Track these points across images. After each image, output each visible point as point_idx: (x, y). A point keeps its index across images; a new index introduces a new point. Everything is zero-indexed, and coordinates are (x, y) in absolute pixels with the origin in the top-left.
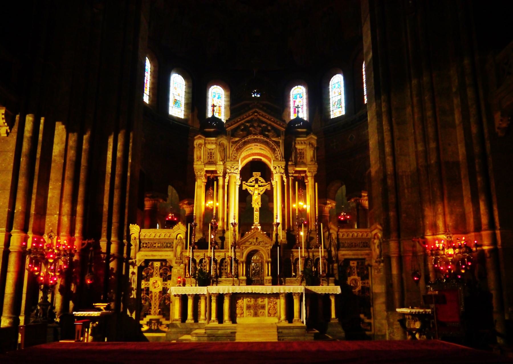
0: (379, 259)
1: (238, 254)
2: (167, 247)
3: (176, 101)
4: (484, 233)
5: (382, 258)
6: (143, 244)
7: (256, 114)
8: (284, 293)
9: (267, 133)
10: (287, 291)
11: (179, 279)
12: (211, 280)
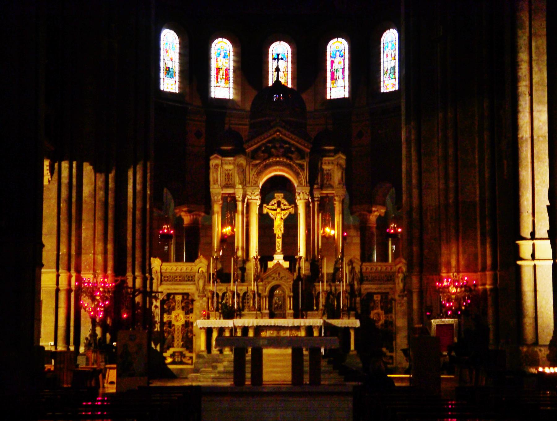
0: (402, 293)
1: (260, 288)
2: (189, 280)
3: (168, 70)
4: (488, 273)
5: (406, 293)
6: (165, 277)
7: (278, 133)
8: (304, 326)
9: (290, 155)
10: (307, 324)
12: (235, 314)
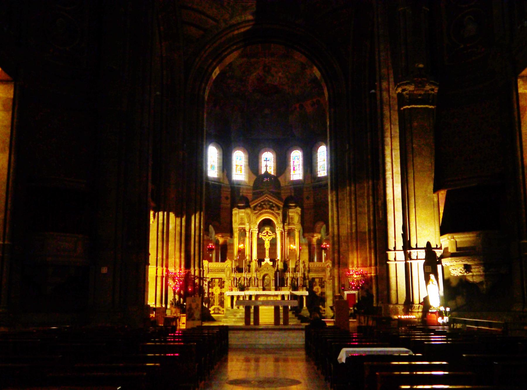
1: (258, 275)
2: (222, 271)
11: (230, 288)
